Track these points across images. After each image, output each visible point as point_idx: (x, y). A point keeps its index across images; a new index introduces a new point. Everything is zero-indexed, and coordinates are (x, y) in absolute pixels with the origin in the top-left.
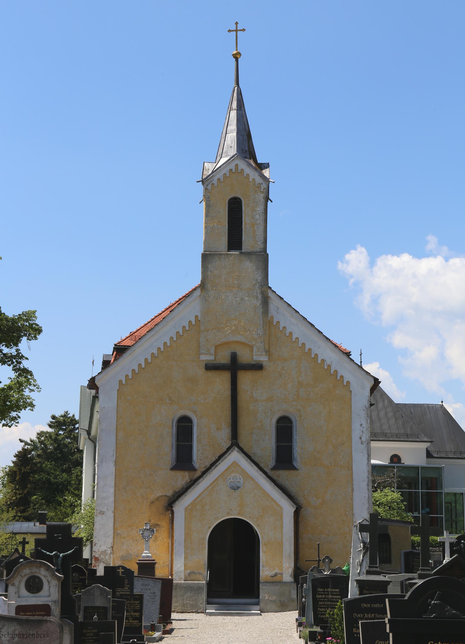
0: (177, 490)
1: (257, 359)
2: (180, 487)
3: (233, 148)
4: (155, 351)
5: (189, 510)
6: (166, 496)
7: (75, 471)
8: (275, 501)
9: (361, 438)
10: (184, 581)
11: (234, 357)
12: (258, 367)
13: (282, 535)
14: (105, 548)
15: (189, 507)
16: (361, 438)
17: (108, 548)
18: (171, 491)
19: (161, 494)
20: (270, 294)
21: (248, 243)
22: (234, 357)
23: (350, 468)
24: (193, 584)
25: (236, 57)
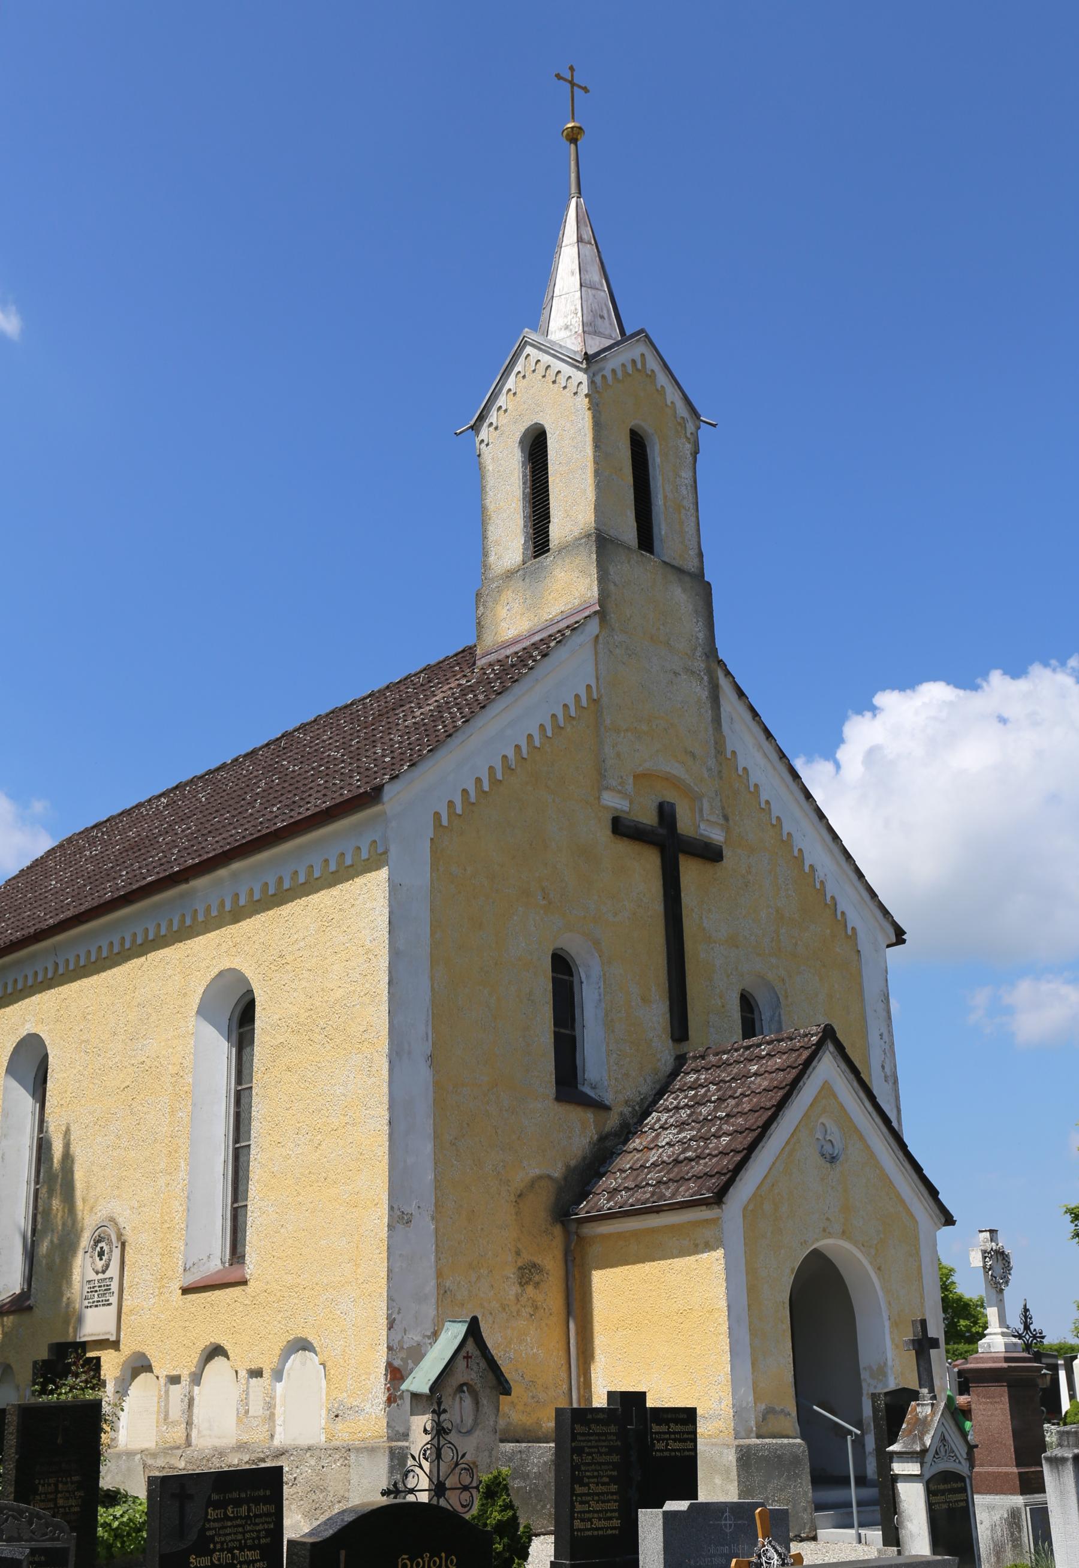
0: (573, 1163)
1: (706, 833)
2: (580, 1153)
4: (511, 753)
5: (751, 1213)
6: (549, 1177)
8: (902, 1202)
9: (883, 1067)
10: (758, 1438)
11: (666, 813)
13: (922, 1297)
14: (418, 1338)
15: (750, 1207)
16: (883, 1067)
17: (424, 1336)
18: (560, 1165)
19: (537, 1172)
22: (666, 813)
24: (782, 1446)
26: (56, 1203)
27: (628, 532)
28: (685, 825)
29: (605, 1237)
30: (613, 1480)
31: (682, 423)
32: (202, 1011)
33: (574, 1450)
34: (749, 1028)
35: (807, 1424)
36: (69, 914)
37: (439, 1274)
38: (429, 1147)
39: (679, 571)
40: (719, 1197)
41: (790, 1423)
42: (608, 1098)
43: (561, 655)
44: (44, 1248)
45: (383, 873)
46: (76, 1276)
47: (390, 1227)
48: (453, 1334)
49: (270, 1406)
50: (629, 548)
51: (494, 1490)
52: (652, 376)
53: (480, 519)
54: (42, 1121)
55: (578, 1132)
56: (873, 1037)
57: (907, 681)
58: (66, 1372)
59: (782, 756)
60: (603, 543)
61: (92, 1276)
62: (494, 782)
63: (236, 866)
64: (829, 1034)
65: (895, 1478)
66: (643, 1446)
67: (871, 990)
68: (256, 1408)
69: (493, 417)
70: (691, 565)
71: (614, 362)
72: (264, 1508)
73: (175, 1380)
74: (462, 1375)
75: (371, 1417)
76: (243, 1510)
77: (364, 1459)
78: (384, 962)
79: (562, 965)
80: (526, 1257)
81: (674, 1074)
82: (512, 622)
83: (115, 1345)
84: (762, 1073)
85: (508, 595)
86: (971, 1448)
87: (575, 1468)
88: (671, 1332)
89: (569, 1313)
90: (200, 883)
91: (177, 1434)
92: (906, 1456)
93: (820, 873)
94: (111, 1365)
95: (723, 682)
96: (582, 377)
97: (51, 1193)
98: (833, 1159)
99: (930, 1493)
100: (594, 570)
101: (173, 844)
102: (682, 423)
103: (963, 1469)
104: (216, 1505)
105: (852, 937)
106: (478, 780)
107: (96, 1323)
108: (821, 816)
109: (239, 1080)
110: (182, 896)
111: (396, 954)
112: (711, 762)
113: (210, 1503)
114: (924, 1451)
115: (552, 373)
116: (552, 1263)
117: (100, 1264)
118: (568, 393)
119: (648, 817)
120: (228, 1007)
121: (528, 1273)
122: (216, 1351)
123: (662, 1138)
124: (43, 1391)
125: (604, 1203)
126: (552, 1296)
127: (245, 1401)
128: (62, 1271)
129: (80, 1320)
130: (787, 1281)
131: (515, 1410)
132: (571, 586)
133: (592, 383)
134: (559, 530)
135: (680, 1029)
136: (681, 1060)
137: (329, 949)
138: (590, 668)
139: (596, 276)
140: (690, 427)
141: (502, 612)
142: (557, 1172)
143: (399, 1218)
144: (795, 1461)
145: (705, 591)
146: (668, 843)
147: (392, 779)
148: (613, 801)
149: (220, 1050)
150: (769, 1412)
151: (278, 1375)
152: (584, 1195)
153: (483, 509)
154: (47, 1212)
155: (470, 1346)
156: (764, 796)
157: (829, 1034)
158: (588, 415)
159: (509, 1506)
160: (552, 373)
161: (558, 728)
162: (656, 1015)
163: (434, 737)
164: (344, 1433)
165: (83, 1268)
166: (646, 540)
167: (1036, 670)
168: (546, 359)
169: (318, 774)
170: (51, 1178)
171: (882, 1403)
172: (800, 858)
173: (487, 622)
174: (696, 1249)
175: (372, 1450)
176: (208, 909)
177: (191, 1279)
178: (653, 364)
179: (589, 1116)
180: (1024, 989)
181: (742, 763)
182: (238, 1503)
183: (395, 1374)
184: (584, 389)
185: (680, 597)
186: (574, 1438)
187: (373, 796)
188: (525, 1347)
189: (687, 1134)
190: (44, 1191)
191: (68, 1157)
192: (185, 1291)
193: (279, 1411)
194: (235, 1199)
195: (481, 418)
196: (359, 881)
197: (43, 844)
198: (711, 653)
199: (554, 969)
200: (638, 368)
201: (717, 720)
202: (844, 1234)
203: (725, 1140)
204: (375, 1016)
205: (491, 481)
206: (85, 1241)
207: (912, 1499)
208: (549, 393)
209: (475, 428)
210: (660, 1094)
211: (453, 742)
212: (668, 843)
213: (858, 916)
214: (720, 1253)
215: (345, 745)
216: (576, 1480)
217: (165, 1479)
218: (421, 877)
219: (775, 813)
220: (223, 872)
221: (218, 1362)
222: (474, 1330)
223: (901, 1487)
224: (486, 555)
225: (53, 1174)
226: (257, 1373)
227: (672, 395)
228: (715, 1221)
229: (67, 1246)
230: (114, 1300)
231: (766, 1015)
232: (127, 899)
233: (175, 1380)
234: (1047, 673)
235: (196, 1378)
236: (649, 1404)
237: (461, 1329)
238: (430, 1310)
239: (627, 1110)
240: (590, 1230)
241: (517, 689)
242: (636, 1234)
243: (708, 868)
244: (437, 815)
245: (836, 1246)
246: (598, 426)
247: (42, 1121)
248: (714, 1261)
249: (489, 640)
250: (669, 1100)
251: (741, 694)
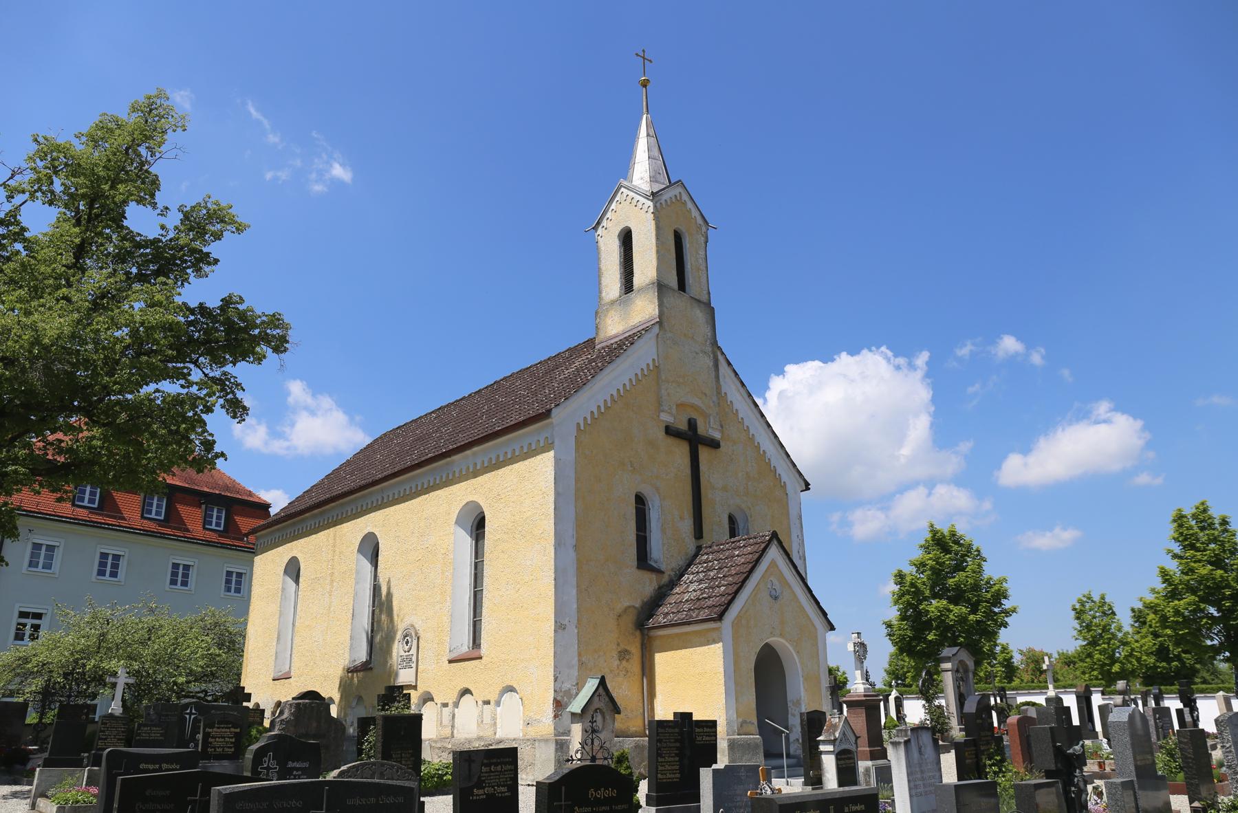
4: (615, 394)
5: (736, 624)
11: (692, 424)
22: (692, 424)
26: (384, 617)
27: (673, 281)
28: (702, 430)
29: (661, 636)
30: (677, 755)
31: (700, 227)
32: (458, 522)
33: (658, 741)
34: (733, 533)
35: (762, 728)
36: (389, 472)
37: (580, 655)
38: (575, 591)
39: (699, 301)
40: (720, 617)
41: (754, 728)
42: (663, 568)
43: (640, 344)
44: (378, 638)
45: (552, 453)
46: (394, 654)
47: (555, 631)
48: (591, 685)
49: (494, 719)
51: (622, 759)
52: (685, 203)
53: (598, 274)
54: (376, 576)
55: (648, 585)
56: (794, 537)
57: (799, 359)
58: (394, 700)
59: (750, 395)
60: (661, 287)
61: (402, 653)
62: (607, 408)
63: (475, 449)
64: (775, 535)
65: (821, 753)
66: (687, 740)
67: (793, 513)
68: (487, 720)
69: (604, 223)
70: (704, 298)
71: (666, 196)
72: (509, 767)
73: (445, 705)
74: (597, 704)
75: (546, 724)
76: (499, 768)
77: (542, 744)
78: (552, 499)
79: (640, 500)
80: (622, 646)
81: (696, 555)
82: (614, 326)
83: (415, 688)
84: (741, 555)
85: (612, 313)
86: (857, 738)
87: (658, 749)
88: (695, 682)
89: (643, 675)
90: (456, 458)
91: (447, 732)
92: (825, 742)
93: (768, 455)
94: (415, 696)
95: (720, 357)
96: (651, 204)
97: (381, 611)
98: (776, 598)
99: (837, 759)
101: (440, 438)
102: (700, 227)
103: (853, 748)
104: (486, 765)
105: (784, 487)
106: (599, 407)
107: (404, 677)
108: (769, 426)
109: (476, 557)
110: (447, 464)
111: (558, 494)
112: (715, 398)
113: (483, 764)
114: (835, 739)
115: (634, 202)
116: (635, 650)
117: (406, 648)
118: (643, 211)
119: (683, 426)
120: (470, 520)
121: (623, 655)
122: (466, 691)
123: (690, 588)
124: (383, 709)
125: (661, 620)
126: (635, 665)
127: (481, 715)
128: (387, 651)
129: (397, 675)
130: (753, 658)
131: (620, 722)
132: (644, 309)
133: (655, 206)
134: (638, 280)
135: (698, 533)
136: (699, 548)
137: (524, 492)
138: (655, 350)
139: (656, 153)
140: (704, 229)
141: (609, 321)
143: (559, 627)
144: (757, 746)
145: (711, 312)
146: (693, 439)
147: (557, 405)
148: (666, 418)
149: (467, 542)
150: (744, 723)
151: (498, 703)
152: (651, 616)
153: (599, 269)
154: (379, 621)
155: (601, 690)
156: (740, 416)
157: (775, 535)
158: (653, 223)
159: (629, 767)
160: (634, 202)
161: (638, 381)
162: (687, 525)
163: (576, 385)
164: (532, 732)
165: (398, 649)
166: (682, 286)
167: (865, 351)
168: (631, 194)
169: (515, 403)
170: (381, 604)
171: (805, 718)
172: (758, 447)
173: (601, 326)
174: (708, 643)
175: (547, 741)
176: (461, 471)
177: (453, 656)
178: (685, 197)
179: (654, 576)
180: (858, 514)
181: (729, 399)
182: (496, 764)
183: (559, 705)
184: (651, 210)
185: (699, 315)
186: (658, 734)
187: (547, 414)
188: (625, 690)
189: (703, 586)
190: (377, 611)
191: (389, 594)
192: (450, 662)
193: (498, 721)
194: (475, 616)
195: (598, 223)
196: (539, 457)
197: (368, 441)
198: (714, 343)
199: (636, 502)
200: (677, 199)
201: (717, 377)
202: (781, 635)
203: (723, 588)
204: (547, 526)
205: (603, 255)
206: (399, 636)
207: (829, 764)
208: (633, 211)
209: (595, 228)
210: (689, 565)
211: (586, 388)
212: (693, 439)
214: (720, 644)
215: (529, 388)
216: (659, 755)
217: (461, 752)
218: (570, 456)
220: (468, 452)
221: (468, 696)
222: (603, 682)
223: (824, 757)
224: (600, 292)
225: (381, 604)
226: (488, 703)
227: (695, 213)
228: (717, 629)
229: (389, 638)
230: (414, 665)
231: (741, 525)
232: (420, 465)
233: (445, 705)
234: (869, 355)
235: (456, 705)
236: (694, 718)
237: (597, 681)
238: (575, 672)
240: (653, 633)
241: (618, 361)
242: (677, 635)
243: (713, 451)
244: (578, 424)
245: (772, 640)
246: (658, 228)
247: (376, 576)
248: (717, 649)
249: (602, 336)
250: (694, 569)
251: (729, 364)
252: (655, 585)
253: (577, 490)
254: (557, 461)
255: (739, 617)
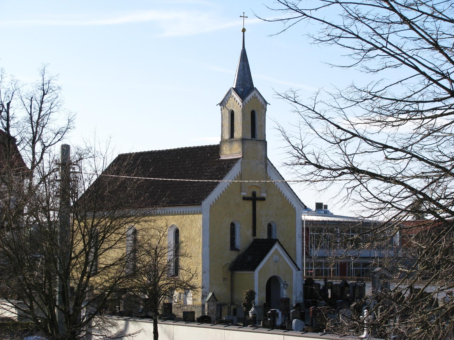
3: (137, 226)
4: (224, 190)
7: (238, 84)
11: (254, 194)
12: (263, 199)
19: (226, 263)
20: (268, 162)
21: (258, 136)
22: (254, 194)
23: (295, 250)
25: (244, 30)
27: (249, 136)
48: (210, 294)
50: (249, 140)
79: (233, 225)
93: (288, 198)
100: (241, 147)
142: (230, 262)
148: (244, 194)
179: (236, 252)
213: (296, 205)
219: (278, 187)
239: (243, 250)
252: (237, 255)
253: (210, 227)
254: (203, 219)
255: (261, 270)
